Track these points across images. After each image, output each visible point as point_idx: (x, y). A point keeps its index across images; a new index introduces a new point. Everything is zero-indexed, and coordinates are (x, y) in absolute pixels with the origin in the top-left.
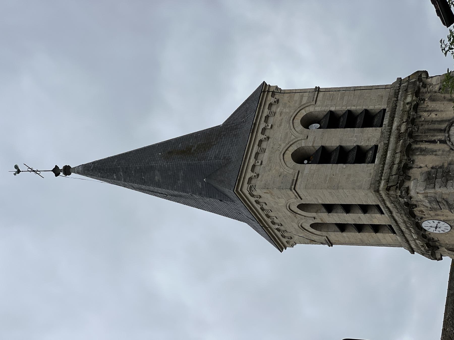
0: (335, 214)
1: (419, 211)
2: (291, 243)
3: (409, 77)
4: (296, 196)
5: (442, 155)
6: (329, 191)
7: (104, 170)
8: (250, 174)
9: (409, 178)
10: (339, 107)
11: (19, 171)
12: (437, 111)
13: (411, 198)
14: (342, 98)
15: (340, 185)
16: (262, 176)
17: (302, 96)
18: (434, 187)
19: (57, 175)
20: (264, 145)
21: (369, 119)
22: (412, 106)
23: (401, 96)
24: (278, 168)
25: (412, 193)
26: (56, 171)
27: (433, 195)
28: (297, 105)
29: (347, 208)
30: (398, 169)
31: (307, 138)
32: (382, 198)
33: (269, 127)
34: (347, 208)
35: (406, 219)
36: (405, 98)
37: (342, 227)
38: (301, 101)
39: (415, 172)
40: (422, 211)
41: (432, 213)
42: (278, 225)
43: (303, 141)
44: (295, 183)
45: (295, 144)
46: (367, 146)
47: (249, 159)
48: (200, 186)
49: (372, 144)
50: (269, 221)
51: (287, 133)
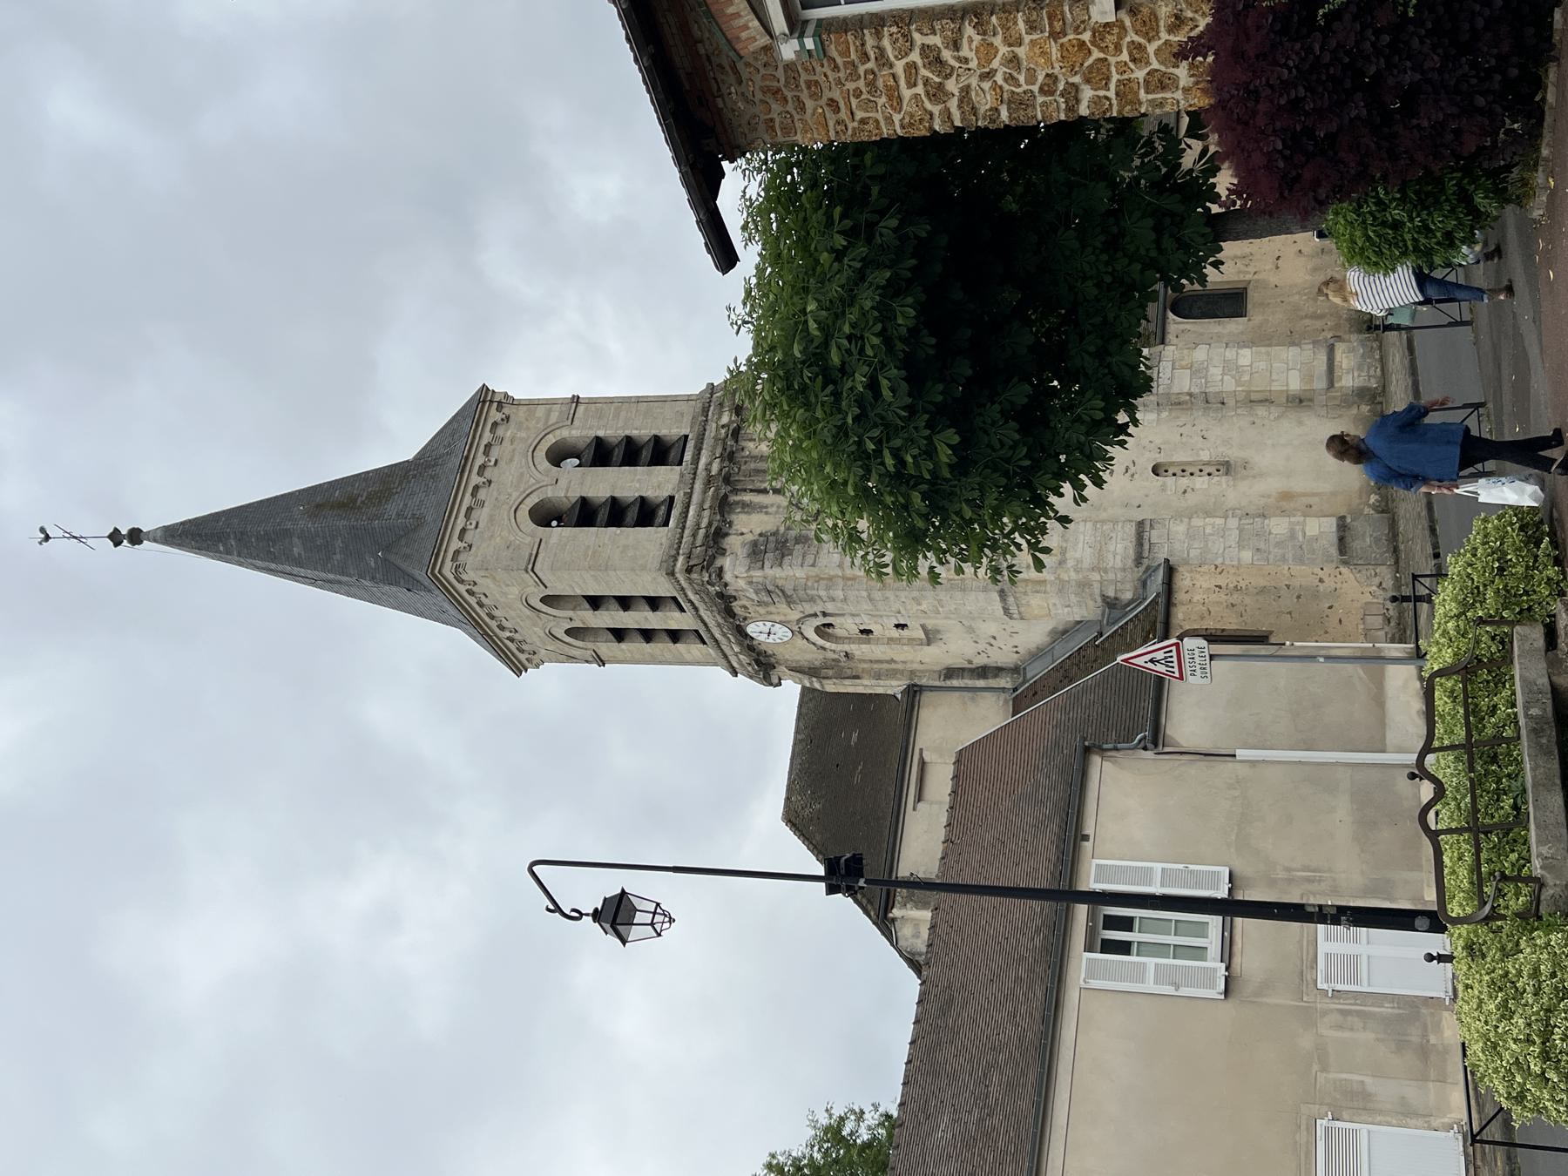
8: (456, 544)
9: (723, 552)
10: (613, 431)
11: (47, 538)
13: (726, 585)
17: (550, 411)
19: (117, 544)
20: (482, 494)
21: (661, 452)
24: (505, 533)
25: (728, 577)
26: (116, 538)
28: (540, 425)
29: (625, 603)
30: (706, 536)
34: (625, 603)
35: (721, 621)
39: (733, 542)
50: (493, 624)
51: (522, 475)
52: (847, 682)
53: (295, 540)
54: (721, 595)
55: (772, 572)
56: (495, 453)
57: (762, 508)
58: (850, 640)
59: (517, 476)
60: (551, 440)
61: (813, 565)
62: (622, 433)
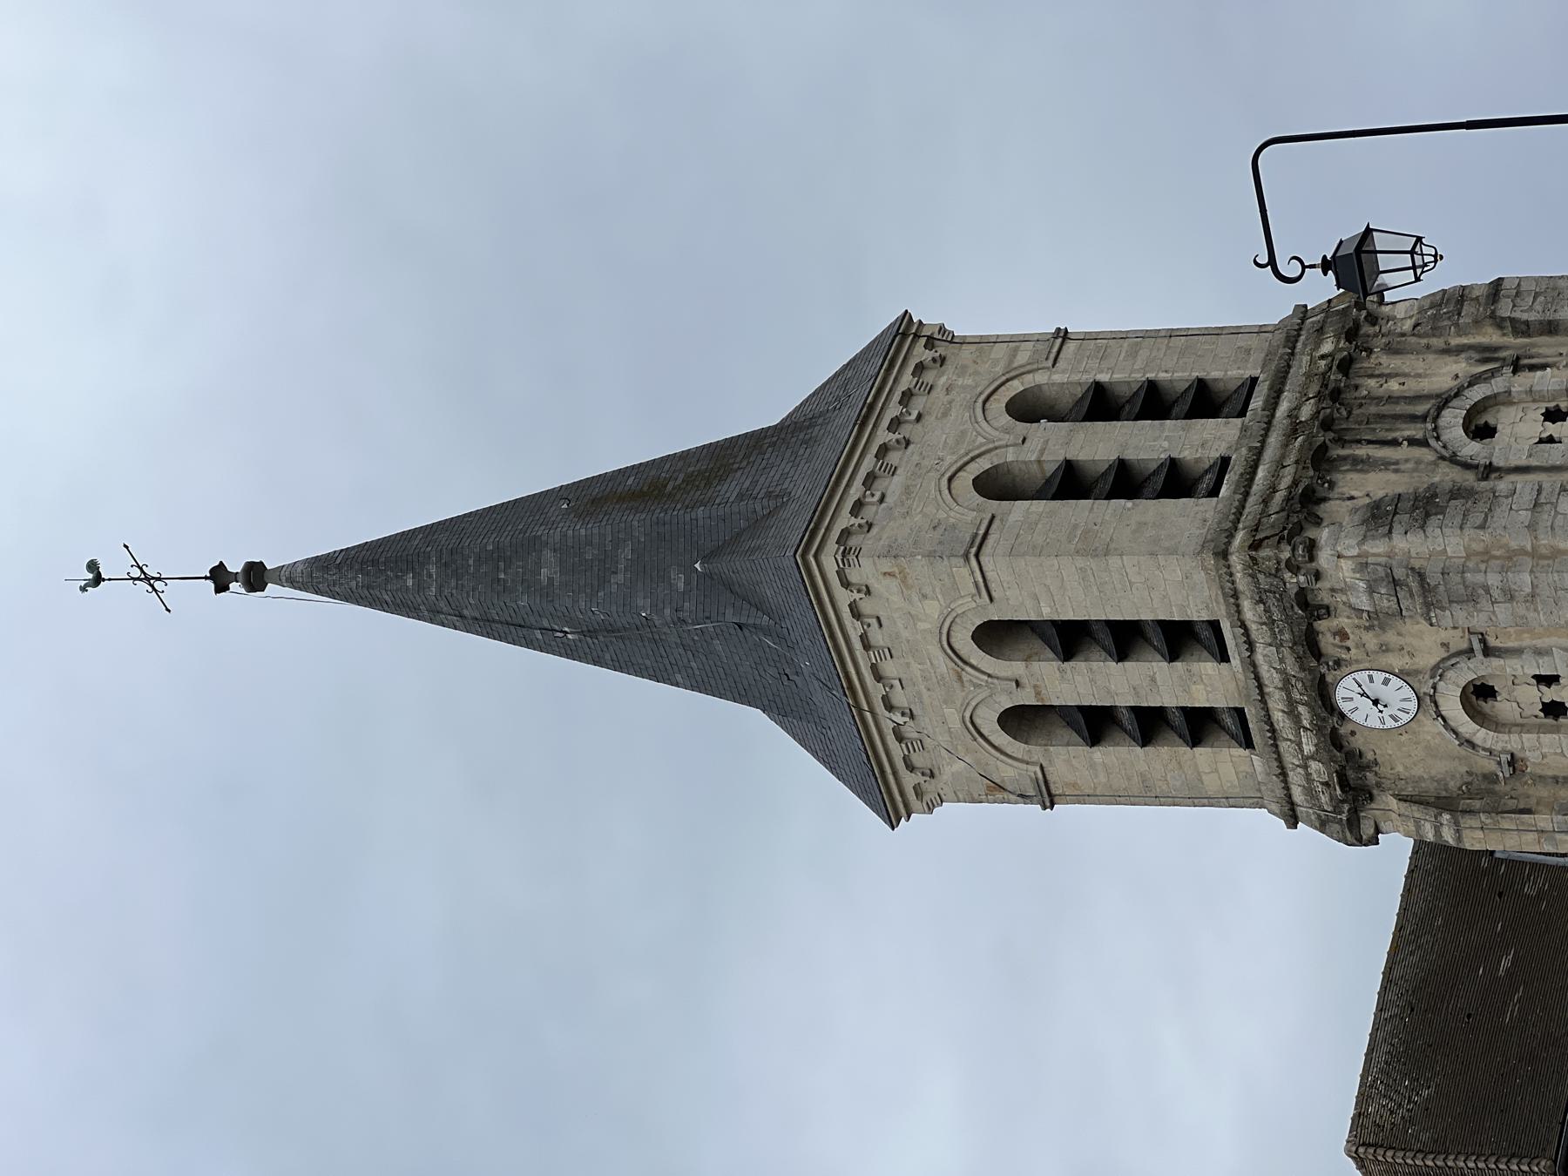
0: (1083, 664)
1: (1335, 634)
2: (926, 798)
3: (1329, 301)
4: (976, 584)
5: (1415, 470)
6: (1080, 562)
7: (376, 574)
8: (845, 520)
9: (1318, 522)
10: (1123, 374)
11: (98, 580)
12: (1406, 375)
13: (1318, 576)
14: (1133, 354)
15: (1112, 546)
16: (883, 528)
17: (1016, 350)
18: (1390, 532)
19: (221, 588)
20: (893, 458)
21: (1205, 401)
22: (1336, 363)
23: (1305, 345)
24: (930, 509)
25: (1324, 559)
26: (220, 578)
27: (1383, 560)
28: (999, 369)
29: (1124, 638)
30: (1288, 499)
31: (1024, 440)
32: (1233, 583)
33: (913, 417)
35: (1292, 668)
36: (1318, 345)
37: (1095, 724)
38: (1011, 362)
39: (1334, 509)
40: (1342, 634)
41: (1371, 641)
42: (903, 714)
43: (1011, 449)
44: (979, 544)
45: (987, 456)
46: (1197, 460)
47: (848, 485)
48: (681, 585)
49: (1214, 455)
50: (877, 691)
51: (963, 433)
52: (1507, 822)
53: (548, 555)
54: (1302, 598)
55: (1409, 545)
56: (918, 404)
57: (1386, 465)
58: (1522, 727)
59: (956, 427)
60: (1016, 387)
61: (1482, 527)
62: (1140, 377)
